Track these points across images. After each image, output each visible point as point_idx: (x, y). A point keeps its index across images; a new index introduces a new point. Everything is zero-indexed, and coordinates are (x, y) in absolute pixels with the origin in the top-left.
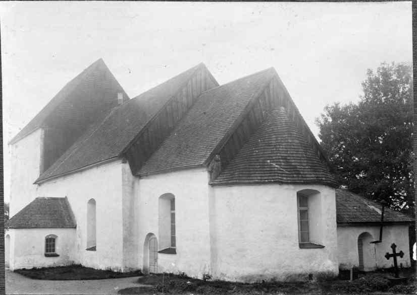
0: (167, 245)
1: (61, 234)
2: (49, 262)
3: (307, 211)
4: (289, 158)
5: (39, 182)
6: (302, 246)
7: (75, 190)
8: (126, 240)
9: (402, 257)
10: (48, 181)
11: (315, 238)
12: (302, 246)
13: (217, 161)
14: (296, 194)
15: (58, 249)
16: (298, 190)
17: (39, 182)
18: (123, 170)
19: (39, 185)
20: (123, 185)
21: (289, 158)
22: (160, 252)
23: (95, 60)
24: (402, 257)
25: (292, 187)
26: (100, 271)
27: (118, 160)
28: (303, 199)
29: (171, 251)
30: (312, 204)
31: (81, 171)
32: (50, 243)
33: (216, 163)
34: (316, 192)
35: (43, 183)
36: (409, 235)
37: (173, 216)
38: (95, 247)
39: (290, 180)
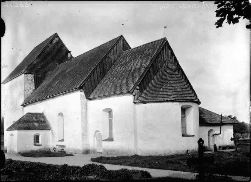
0: (107, 137)
1: (41, 133)
2: (36, 148)
3: (185, 117)
4: (176, 88)
5: (24, 105)
6: (183, 135)
7: (48, 108)
8: (83, 135)
9: (232, 138)
10: (30, 103)
11: (189, 132)
12: (183, 135)
13: (137, 90)
14: (180, 107)
15: (40, 142)
16: (181, 105)
17: (24, 105)
18: (81, 96)
19: (24, 106)
20: (81, 104)
21: (176, 88)
22: (103, 141)
23: (215, 5)
24: (232, 138)
25: (178, 103)
26: (69, 154)
27: (78, 90)
28: (184, 110)
29: (111, 140)
30: (187, 112)
31: (53, 97)
32: (37, 138)
33: (137, 91)
34: (190, 107)
35: (27, 105)
36: (234, 128)
37: (110, 121)
38: (90, 154)
39: (154, 95)
